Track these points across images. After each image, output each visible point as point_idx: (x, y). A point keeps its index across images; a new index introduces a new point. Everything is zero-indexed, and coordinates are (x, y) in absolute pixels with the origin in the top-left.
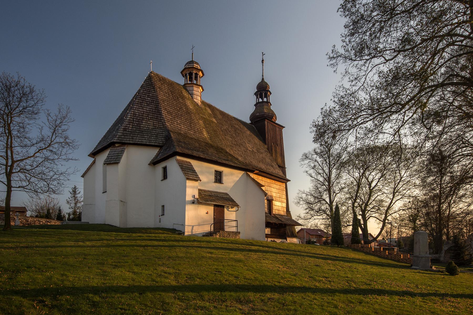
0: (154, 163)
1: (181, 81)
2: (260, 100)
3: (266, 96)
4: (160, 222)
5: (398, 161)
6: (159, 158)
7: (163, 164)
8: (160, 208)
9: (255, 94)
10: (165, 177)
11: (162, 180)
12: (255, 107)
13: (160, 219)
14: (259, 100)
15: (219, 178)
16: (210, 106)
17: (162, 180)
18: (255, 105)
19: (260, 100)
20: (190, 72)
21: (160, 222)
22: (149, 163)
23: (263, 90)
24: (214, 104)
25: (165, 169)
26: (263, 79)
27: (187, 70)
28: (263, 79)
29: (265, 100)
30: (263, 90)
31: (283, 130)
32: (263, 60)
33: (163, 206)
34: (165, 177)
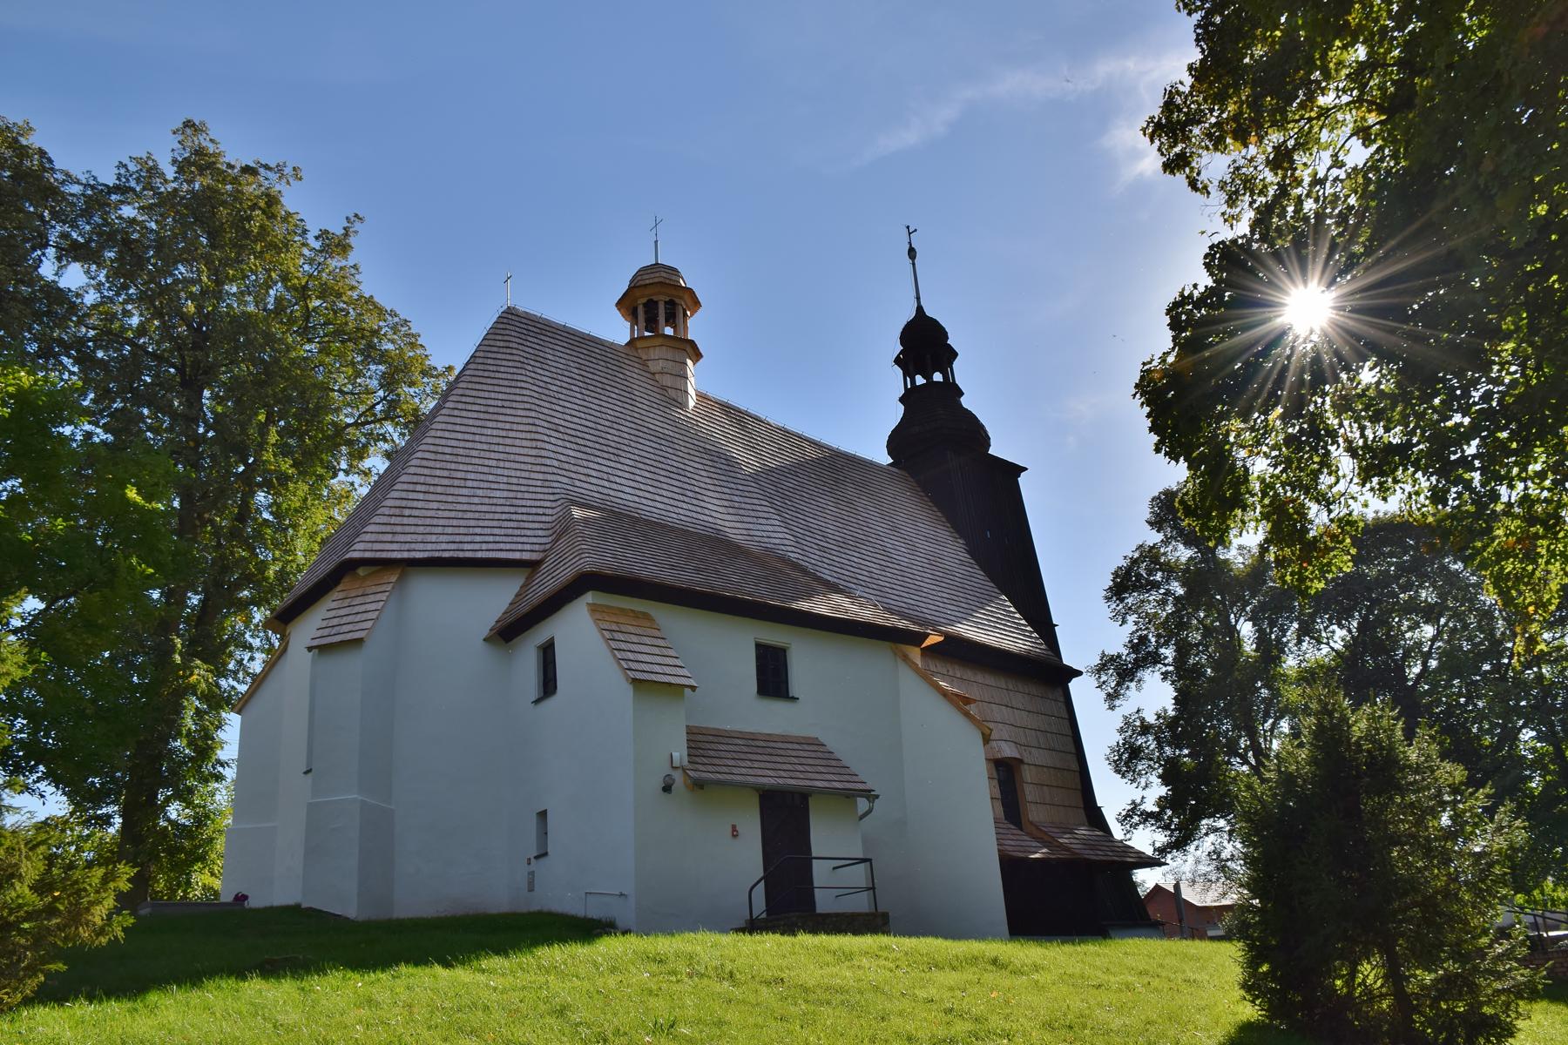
0: (508, 632)
1: (617, 330)
2: (920, 380)
3: (671, 319)
4: (531, 889)
5: (1310, 120)
6: (525, 608)
7: (540, 634)
8: (532, 824)
9: (897, 361)
10: (548, 685)
11: (537, 702)
12: (902, 407)
13: (532, 873)
14: (913, 381)
15: (773, 677)
16: (726, 408)
17: (537, 702)
18: (901, 400)
19: (920, 380)
20: (650, 301)
21: (531, 889)
22: (486, 632)
23: (925, 345)
24: (735, 402)
25: (548, 653)
26: (920, 309)
27: (638, 293)
28: (920, 309)
29: (938, 377)
30: (925, 345)
31: (1023, 480)
32: (912, 253)
33: (543, 815)
34: (548, 685)
